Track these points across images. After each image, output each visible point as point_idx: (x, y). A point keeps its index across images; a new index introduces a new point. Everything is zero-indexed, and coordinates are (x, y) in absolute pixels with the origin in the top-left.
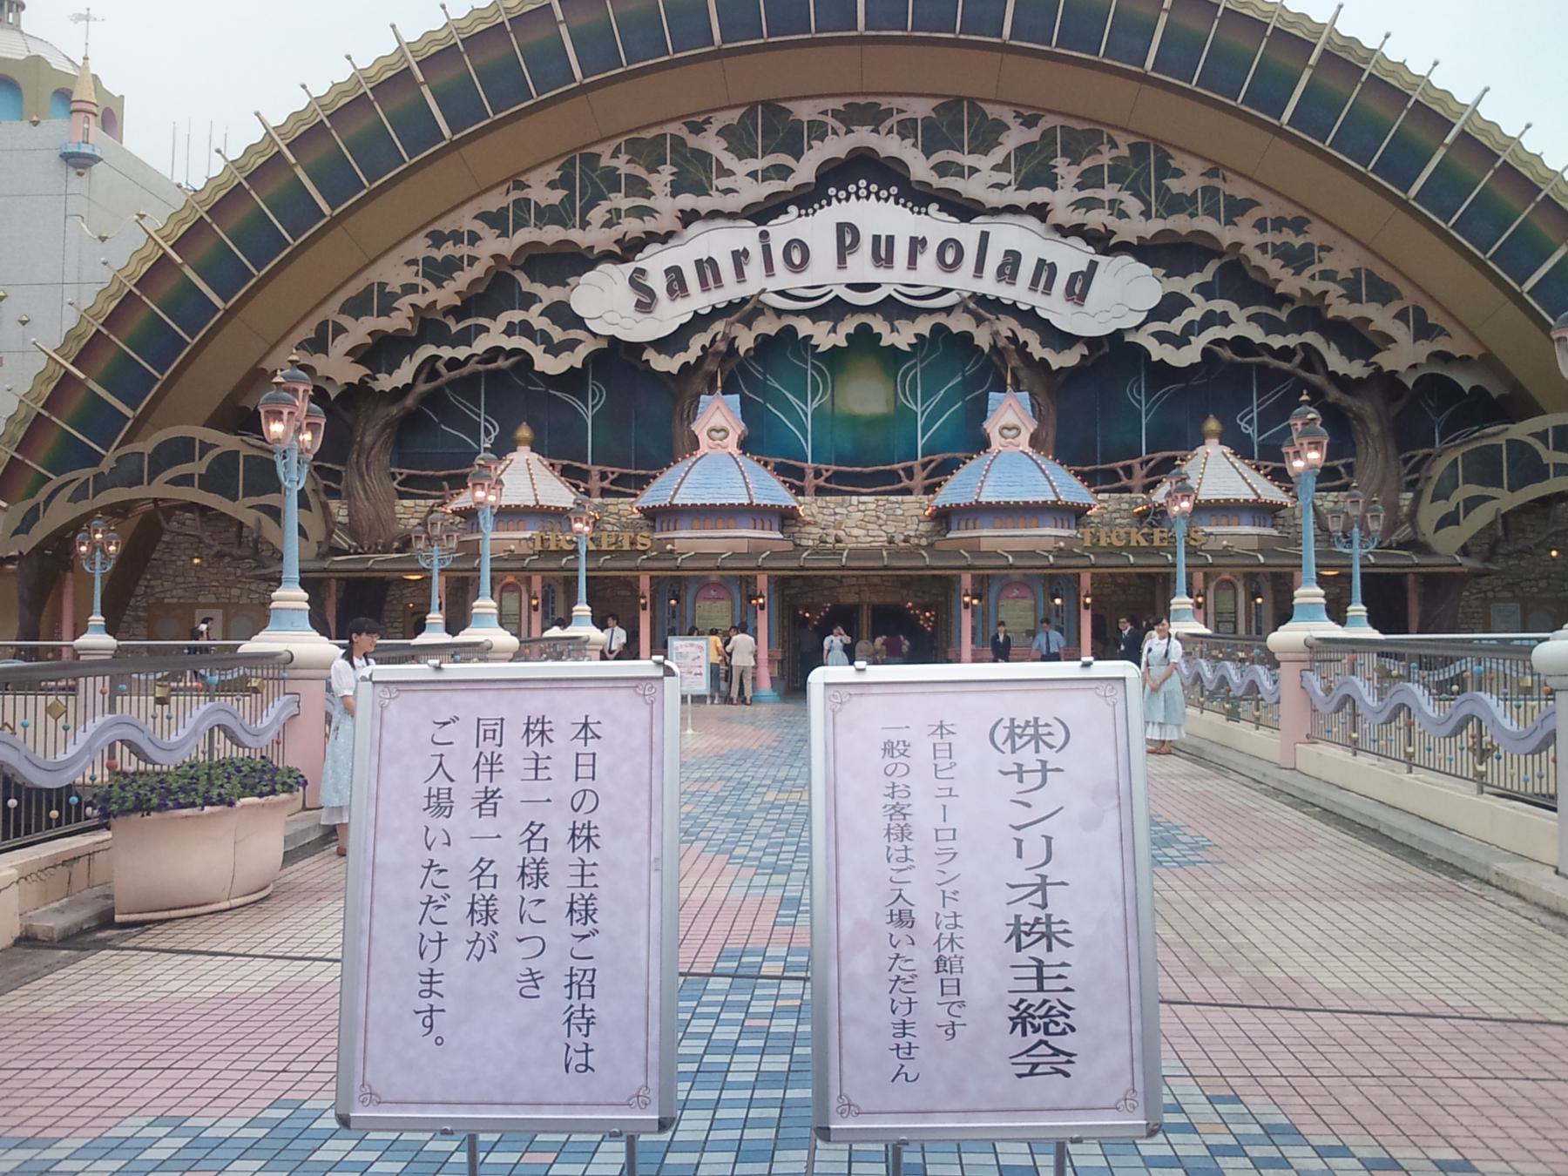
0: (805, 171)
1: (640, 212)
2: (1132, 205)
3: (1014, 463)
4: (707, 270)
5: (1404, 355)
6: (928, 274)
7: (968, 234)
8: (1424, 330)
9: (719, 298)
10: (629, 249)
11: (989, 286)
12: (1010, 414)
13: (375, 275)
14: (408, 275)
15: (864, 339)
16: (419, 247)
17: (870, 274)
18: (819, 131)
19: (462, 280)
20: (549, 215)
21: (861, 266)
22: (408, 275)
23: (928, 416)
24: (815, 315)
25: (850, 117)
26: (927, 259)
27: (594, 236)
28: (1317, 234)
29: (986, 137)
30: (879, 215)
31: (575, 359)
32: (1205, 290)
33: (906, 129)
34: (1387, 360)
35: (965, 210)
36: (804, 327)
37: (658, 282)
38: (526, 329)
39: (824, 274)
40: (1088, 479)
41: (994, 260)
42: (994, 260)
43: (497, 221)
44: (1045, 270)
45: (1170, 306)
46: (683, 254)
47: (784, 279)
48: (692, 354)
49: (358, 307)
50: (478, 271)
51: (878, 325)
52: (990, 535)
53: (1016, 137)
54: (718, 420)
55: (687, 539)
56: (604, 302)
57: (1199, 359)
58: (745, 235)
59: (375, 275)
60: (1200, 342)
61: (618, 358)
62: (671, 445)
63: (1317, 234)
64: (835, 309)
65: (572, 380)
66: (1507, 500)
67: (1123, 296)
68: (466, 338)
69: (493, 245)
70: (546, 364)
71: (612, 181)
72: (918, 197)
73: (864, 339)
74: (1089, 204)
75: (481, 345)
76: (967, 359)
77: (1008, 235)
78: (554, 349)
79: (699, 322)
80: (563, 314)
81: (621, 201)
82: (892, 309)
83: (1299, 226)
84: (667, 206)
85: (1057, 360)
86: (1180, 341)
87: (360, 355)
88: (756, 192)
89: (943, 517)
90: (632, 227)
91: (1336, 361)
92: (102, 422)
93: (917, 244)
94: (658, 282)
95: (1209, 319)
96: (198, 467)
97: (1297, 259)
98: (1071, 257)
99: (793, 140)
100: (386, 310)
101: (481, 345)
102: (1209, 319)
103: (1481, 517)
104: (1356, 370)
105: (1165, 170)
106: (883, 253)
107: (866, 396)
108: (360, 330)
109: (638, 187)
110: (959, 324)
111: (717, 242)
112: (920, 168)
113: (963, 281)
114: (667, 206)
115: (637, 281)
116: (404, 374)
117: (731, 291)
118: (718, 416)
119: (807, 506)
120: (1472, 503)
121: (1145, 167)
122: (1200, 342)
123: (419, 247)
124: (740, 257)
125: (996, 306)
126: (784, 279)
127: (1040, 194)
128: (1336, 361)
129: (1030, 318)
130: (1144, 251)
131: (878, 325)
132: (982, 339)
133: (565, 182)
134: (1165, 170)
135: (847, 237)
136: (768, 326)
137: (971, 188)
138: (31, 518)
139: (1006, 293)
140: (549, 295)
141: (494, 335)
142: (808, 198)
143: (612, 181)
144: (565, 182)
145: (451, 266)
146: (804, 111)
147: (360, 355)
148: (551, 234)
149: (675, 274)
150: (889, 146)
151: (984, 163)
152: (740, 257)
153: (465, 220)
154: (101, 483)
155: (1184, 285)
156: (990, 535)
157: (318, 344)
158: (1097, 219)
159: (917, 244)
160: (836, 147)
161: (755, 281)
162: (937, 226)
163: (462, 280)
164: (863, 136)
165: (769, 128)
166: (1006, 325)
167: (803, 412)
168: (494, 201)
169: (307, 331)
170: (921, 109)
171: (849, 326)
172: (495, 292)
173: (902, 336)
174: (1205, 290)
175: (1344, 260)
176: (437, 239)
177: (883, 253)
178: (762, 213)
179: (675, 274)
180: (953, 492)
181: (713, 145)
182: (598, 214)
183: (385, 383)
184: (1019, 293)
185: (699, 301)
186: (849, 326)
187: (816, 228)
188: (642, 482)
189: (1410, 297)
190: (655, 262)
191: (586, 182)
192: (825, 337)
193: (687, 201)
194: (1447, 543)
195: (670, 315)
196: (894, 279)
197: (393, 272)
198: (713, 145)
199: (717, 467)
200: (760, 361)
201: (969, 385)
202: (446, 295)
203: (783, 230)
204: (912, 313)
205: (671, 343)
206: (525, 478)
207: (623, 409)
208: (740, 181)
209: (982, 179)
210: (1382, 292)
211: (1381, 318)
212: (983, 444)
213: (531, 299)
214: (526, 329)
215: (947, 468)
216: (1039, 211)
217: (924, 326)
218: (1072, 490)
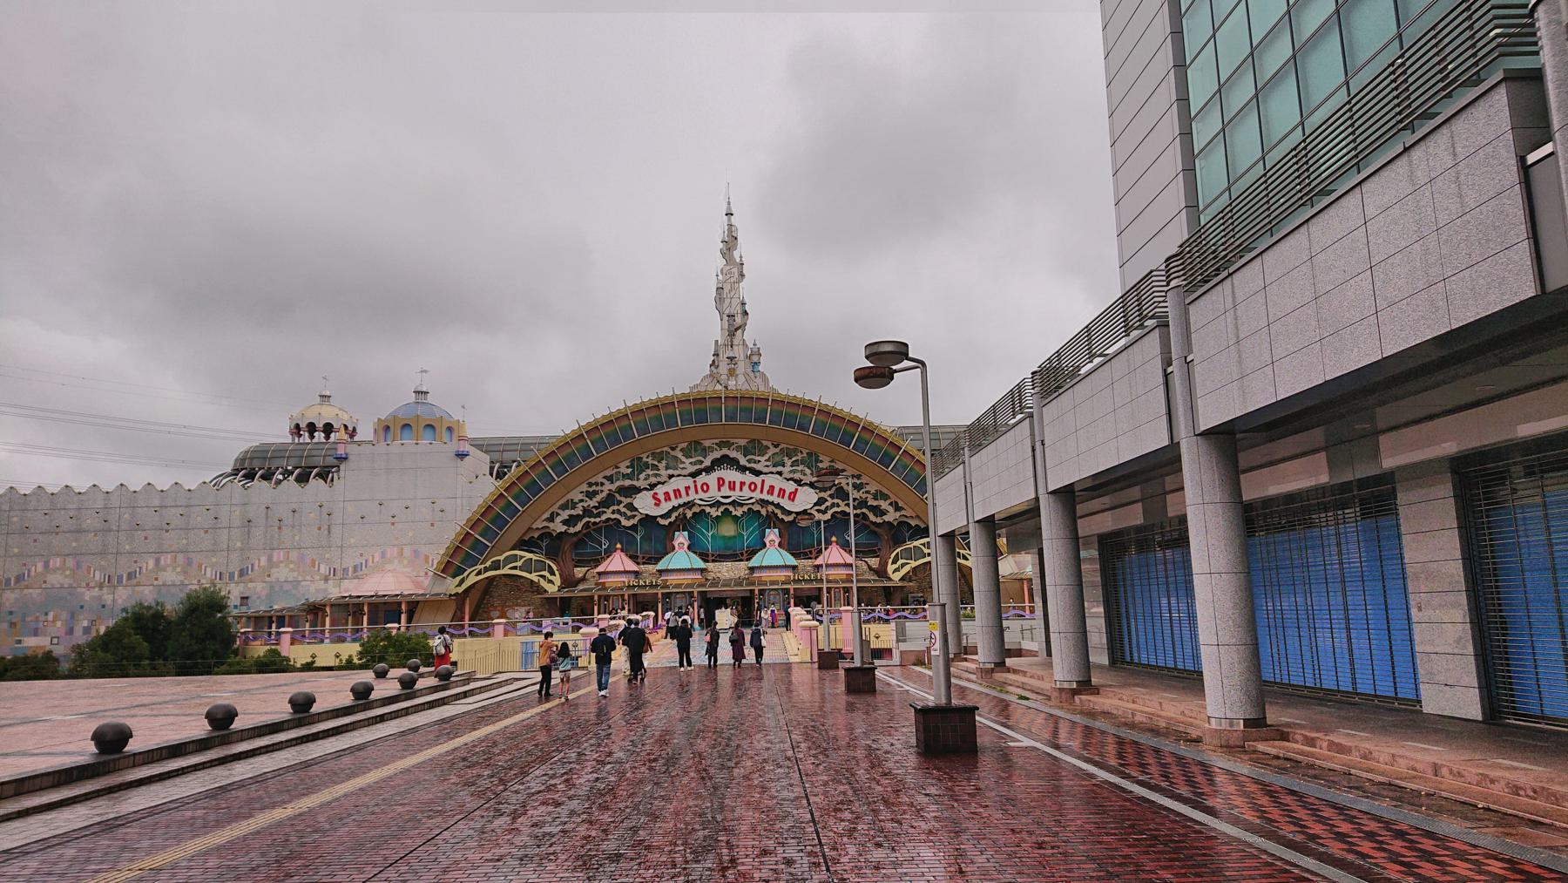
0: (707, 462)
1: (656, 475)
2: (808, 471)
3: (773, 555)
4: (677, 493)
5: (892, 516)
6: (746, 493)
7: (758, 480)
8: (898, 508)
9: (681, 501)
10: (653, 486)
11: (765, 496)
12: (772, 535)
13: (569, 497)
14: (581, 497)
15: (727, 512)
16: (584, 487)
17: (729, 493)
18: (711, 449)
19: (598, 498)
20: (625, 476)
21: (725, 491)
22: (581, 497)
23: (748, 537)
24: (711, 506)
25: (721, 445)
26: (746, 488)
27: (641, 483)
28: (864, 479)
29: (763, 450)
30: (731, 475)
31: (635, 521)
32: (831, 496)
33: (738, 448)
34: (886, 518)
35: (757, 473)
36: (708, 509)
37: (661, 497)
38: (619, 512)
39: (714, 493)
40: (796, 556)
41: (766, 488)
42: (766, 488)
43: (610, 479)
44: (782, 492)
45: (821, 501)
46: (669, 487)
47: (701, 495)
48: (672, 519)
49: (564, 507)
50: (604, 495)
51: (731, 508)
52: (765, 575)
53: (772, 450)
54: (681, 540)
55: (673, 579)
56: (644, 504)
57: (717, 612)
58: (689, 481)
59: (569, 497)
60: (830, 512)
61: (649, 520)
62: (668, 549)
63: (864, 479)
64: (718, 504)
65: (634, 527)
66: (914, 564)
67: (806, 499)
68: (599, 515)
69: (608, 486)
70: (625, 522)
71: (647, 466)
72: (743, 469)
73: (727, 512)
74: (794, 472)
75: (604, 517)
76: (764, 517)
77: (771, 480)
78: (628, 518)
79: (674, 509)
80: (631, 507)
81: (649, 472)
82: (734, 503)
83: (859, 477)
84: (664, 473)
85: (786, 519)
86: (824, 512)
87: (565, 522)
88: (693, 469)
89: (752, 569)
90: (653, 480)
91: (872, 518)
92: (479, 547)
93: (742, 484)
94: (661, 497)
95: (833, 505)
96: (519, 564)
97: (857, 487)
98: (790, 487)
99: (705, 452)
100: (574, 508)
101: (604, 517)
102: (833, 505)
103: (907, 569)
104: (879, 520)
105: (818, 461)
106: (732, 486)
107: (728, 529)
108: (565, 515)
109: (655, 467)
110: (756, 508)
111: (680, 483)
112: (743, 461)
113: (757, 495)
114: (664, 473)
115: (655, 496)
116: (579, 527)
117: (685, 499)
118: (681, 538)
119: (710, 566)
120: (903, 565)
121: (812, 459)
122: (830, 512)
123: (584, 487)
124: (687, 489)
125: (766, 503)
126: (701, 495)
127: (779, 469)
128: (872, 518)
129: (778, 506)
130: (812, 485)
131: (731, 508)
132: (764, 512)
133: (632, 466)
134: (818, 461)
135: (721, 482)
136: (696, 509)
137: (758, 467)
138: (462, 581)
139: (770, 498)
140: (626, 501)
141: (608, 515)
142: (708, 470)
143: (647, 466)
144: (632, 466)
145: (595, 493)
146: (707, 443)
147: (565, 522)
148: (627, 483)
149: (667, 494)
150: (733, 454)
151: (762, 459)
152: (687, 489)
153: (599, 478)
154: (486, 570)
155: (825, 495)
156: (765, 575)
157: (551, 519)
158: (797, 476)
159: (742, 484)
160: (717, 454)
161: (692, 496)
162: (748, 478)
163: (598, 498)
164: (725, 451)
165: (695, 448)
166: (771, 508)
167: (708, 536)
168: (608, 473)
169: (547, 515)
170: (743, 442)
171: (722, 509)
172: (609, 501)
173: (738, 512)
174: (831, 496)
175: (872, 488)
176: (590, 485)
177: (732, 486)
178: (694, 475)
179: (667, 494)
180: (754, 562)
181: (680, 455)
182: (642, 476)
183: (572, 530)
184: (774, 498)
185: (675, 502)
186: (722, 509)
187: (711, 479)
188: (657, 560)
189: (893, 498)
190: (660, 490)
191: (638, 466)
192: (714, 512)
193: (671, 472)
194: (896, 577)
195: (666, 507)
196: (735, 495)
197: (576, 495)
198: (680, 455)
199: (681, 558)
200: (690, 520)
201: (760, 525)
202: (593, 503)
203: (701, 479)
204: (742, 505)
205: (667, 515)
206: (618, 562)
207: (652, 539)
208: (687, 465)
209: (762, 463)
210: (885, 497)
211: (884, 505)
212: (764, 545)
213: (620, 502)
214: (619, 512)
215: (754, 552)
216: (780, 473)
217: (745, 509)
218: (791, 561)
